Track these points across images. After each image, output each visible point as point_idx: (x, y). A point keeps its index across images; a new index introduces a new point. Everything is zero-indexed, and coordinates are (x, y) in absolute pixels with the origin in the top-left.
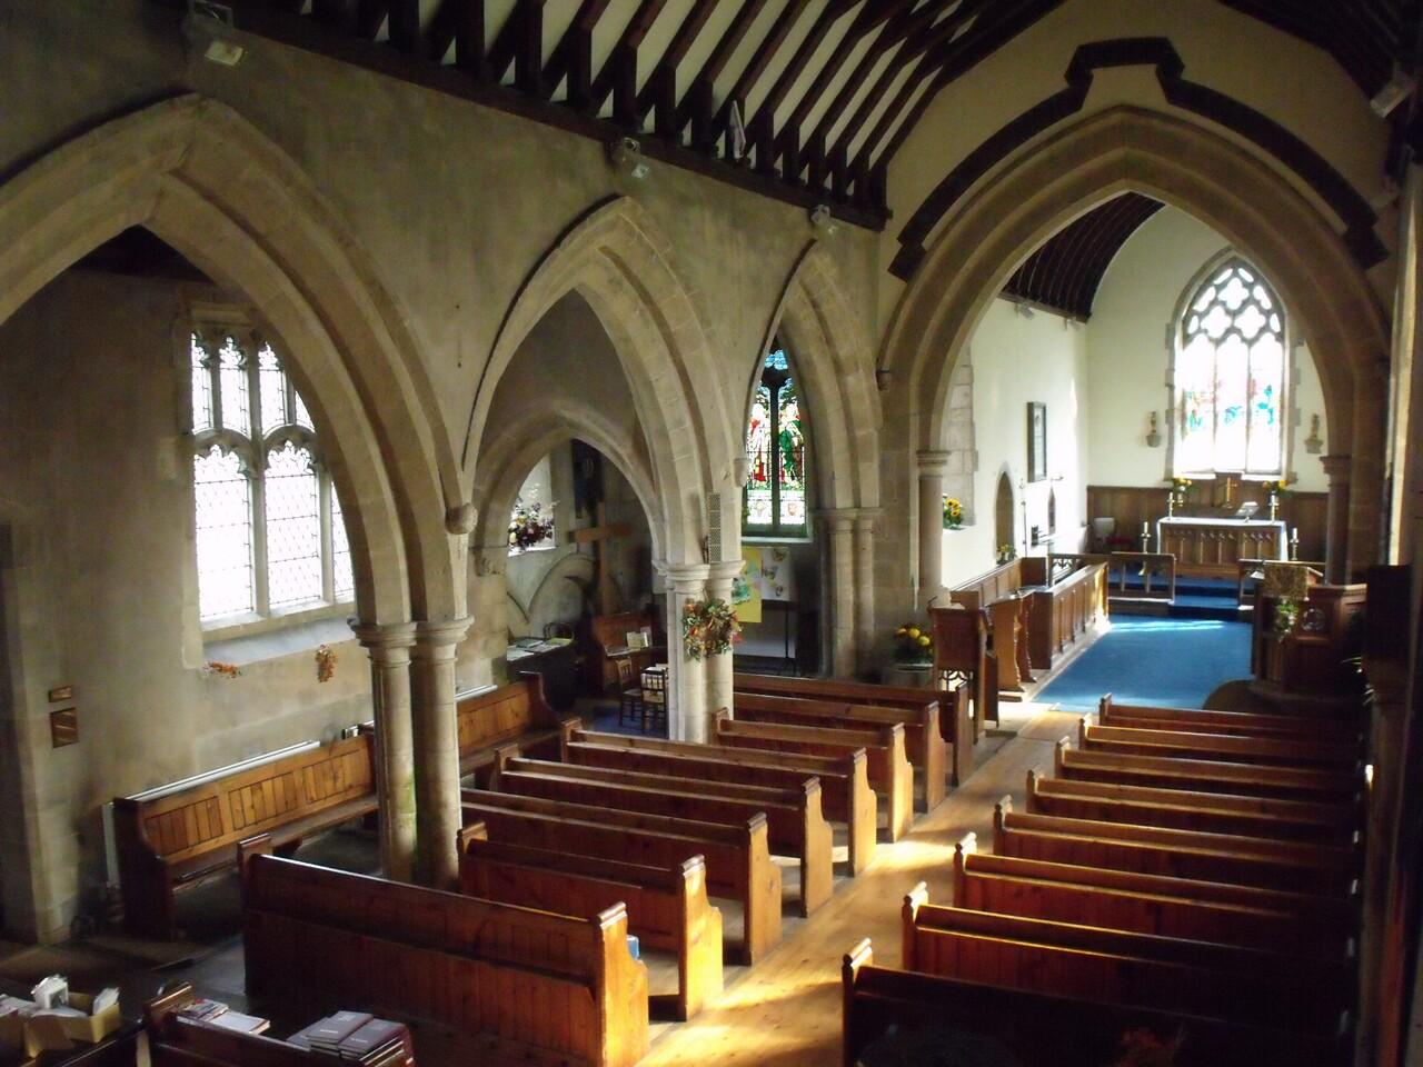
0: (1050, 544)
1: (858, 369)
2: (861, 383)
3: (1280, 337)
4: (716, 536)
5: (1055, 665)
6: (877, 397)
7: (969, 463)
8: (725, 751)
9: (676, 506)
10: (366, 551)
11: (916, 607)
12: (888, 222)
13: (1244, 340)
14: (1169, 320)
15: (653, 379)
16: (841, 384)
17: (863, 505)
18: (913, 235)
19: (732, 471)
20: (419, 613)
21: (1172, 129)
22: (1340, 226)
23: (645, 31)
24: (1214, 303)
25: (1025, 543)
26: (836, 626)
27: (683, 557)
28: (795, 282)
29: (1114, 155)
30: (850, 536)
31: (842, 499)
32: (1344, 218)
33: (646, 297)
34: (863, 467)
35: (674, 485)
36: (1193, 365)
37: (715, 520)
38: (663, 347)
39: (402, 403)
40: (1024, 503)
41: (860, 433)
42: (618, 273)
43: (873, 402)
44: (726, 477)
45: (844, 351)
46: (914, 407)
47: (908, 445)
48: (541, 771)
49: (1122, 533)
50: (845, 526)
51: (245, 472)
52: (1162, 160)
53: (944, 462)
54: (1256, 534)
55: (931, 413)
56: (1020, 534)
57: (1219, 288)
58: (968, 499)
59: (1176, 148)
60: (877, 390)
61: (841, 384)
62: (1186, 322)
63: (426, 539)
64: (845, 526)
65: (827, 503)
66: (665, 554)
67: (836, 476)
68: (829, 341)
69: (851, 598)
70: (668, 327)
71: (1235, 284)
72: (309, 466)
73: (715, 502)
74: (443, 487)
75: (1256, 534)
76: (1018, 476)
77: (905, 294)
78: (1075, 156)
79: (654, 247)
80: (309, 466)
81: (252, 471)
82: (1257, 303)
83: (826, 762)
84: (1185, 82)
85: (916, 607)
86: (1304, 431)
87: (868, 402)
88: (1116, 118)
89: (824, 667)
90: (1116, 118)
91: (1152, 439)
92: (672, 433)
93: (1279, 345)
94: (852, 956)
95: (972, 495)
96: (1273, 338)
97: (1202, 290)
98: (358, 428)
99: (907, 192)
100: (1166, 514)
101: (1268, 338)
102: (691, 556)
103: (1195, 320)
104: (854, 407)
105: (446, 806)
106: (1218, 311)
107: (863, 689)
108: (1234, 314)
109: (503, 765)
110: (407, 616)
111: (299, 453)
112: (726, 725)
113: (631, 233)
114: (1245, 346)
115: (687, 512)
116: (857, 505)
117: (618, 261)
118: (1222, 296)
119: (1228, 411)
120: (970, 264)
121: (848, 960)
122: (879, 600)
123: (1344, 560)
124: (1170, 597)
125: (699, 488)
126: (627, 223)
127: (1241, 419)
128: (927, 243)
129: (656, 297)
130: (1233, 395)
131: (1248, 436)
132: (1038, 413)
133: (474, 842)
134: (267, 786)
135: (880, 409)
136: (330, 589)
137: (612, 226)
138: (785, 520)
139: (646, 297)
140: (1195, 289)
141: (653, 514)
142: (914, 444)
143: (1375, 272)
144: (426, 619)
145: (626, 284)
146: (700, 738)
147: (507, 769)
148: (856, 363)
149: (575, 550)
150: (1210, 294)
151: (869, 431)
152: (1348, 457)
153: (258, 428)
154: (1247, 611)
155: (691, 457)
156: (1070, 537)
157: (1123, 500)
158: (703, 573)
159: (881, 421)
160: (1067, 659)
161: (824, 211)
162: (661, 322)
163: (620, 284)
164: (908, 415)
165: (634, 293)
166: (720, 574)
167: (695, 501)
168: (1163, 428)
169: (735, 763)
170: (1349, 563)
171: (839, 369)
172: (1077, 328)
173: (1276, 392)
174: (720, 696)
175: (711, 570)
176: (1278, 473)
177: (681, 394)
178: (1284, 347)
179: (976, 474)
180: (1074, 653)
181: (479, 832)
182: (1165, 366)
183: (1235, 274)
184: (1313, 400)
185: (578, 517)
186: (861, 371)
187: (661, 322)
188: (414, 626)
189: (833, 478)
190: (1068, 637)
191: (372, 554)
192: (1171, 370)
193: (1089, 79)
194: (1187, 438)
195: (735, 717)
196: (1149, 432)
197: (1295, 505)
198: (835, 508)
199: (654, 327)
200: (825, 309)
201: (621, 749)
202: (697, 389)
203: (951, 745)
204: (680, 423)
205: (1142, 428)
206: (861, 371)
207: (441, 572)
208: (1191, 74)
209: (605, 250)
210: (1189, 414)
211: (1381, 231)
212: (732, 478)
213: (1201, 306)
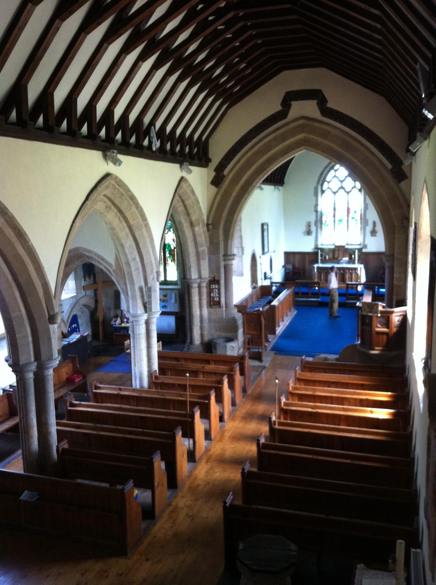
0: (271, 278)
1: (199, 224)
2: (200, 230)
3: (360, 190)
5: (277, 332)
6: (207, 235)
7: (240, 252)
8: (158, 392)
9: (133, 291)
10: (15, 335)
11: (224, 316)
12: (210, 164)
13: (346, 191)
14: (315, 185)
15: (124, 243)
17: (202, 277)
18: (220, 169)
21: (323, 126)
22: (390, 166)
23: (118, 103)
25: (262, 279)
26: (193, 325)
27: (137, 311)
28: (177, 197)
29: (302, 136)
30: (197, 289)
31: (194, 275)
32: (391, 163)
33: (120, 211)
34: (202, 262)
35: (133, 284)
36: (325, 203)
37: (150, 297)
38: (127, 230)
39: (29, 275)
40: (261, 264)
41: (200, 249)
42: (109, 203)
43: (205, 237)
44: (153, 279)
46: (221, 238)
47: (219, 254)
48: (84, 407)
49: (299, 269)
50: (195, 285)
52: (320, 139)
53: (233, 259)
54: (352, 271)
55: (228, 240)
56: (260, 276)
57: (336, 171)
58: (241, 266)
59: (325, 135)
60: (207, 232)
62: (322, 185)
63: (40, 327)
64: (195, 285)
65: (188, 277)
66: (129, 309)
67: (192, 266)
68: (188, 214)
69: (198, 313)
70: (129, 223)
73: (149, 290)
74: (47, 306)
75: (352, 271)
76: (258, 253)
77: (217, 194)
78: (284, 138)
79: (124, 193)
83: (199, 396)
84: (328, 108)
85: (224, 316)
86: (369, 228)
87: (203, 237)
89: (189, 341)
90: (301, 122)
91: (309, 233)
92: (132, 264)
93: (360, 193)
94: (227, 501)
95: (242, 265)
96: (358, 191)
97: (329, 172)
98: (11, 286)
100: (317, 262)
102: (140, 310)
103: (326, 183)
104: (198, 239)
105: (50, 434)
107: (207, 356)
108: (342, 188)
109: (68, 405)
110: (33, 359)
112: (156, 378)
113: (115, 188)
114: (346, 194)
115: (138, 293)
116: (200, 277)
117: (110, 199)
119: (340, 220)
121: (225, 503)
122: (209, 313)
123: (392, 295)
124: (319, 298)
125: (143, 284)
126: (113, 185)
128: (226, 172)
129: (124, 211)
130: (341, 213)
131: (335, 204)
132: (265, 227)
133: (64, 449)
135: (208, 239)
137: (107, 187)
138: (168, 279)
139: (120, 211)
140: (326, 172)
141: (123, 293)
142: (222, 252)
143: (403, 184)
144: (41, 360)
145: (113, 207)
146: (146, 383)
147: (70, 407)
148: (199, 222)
149: (84, 294)
151: (204, 249)
152: (393, 255)
154: (222, 29)
155: (139, 272)
156: (278, 276)
157: (297, 257)
158: (145, 317)
159: (208, 244)
160: (282, 329)
161: (186, 165)
162: (127, 221)
163: (110, 208)
164: (219, 241)
165: (116, 210)
166: (152, 316)
167: (141, 289)
168: (313, 228)
169: (162, 397)
170: (394, 297)
171: (192, 225)
172: (279, 190)
175: (148, 315)
176: (360, 245)
177: (135, 248)
179: (243, 257)
180: (284, 325)
181: (65, 445)
182: (314, 203)
184: (373, 215)
185: (85, 280)
186: (201, 225)
187: (127, 221)
188: (36, 363)
189: (190, 267)
190: (281, 319)
191: (17, 336)
192: (317, 205)
193: (290, 105)
194: (323, 231)
195: (159, 374)
197: (365, 257)
198: (191, 279)
199: (124, 223)
200: (187, 202)
201: (115, 392)
202: (141, 246)
203: (243, 377)
204: (134, 259)
205: (304, 228)
206: (201, 225)
207: (47, 341)
208: (330, 105)
209: (105, 196)
210: (324, 222)
212: (156, 279)
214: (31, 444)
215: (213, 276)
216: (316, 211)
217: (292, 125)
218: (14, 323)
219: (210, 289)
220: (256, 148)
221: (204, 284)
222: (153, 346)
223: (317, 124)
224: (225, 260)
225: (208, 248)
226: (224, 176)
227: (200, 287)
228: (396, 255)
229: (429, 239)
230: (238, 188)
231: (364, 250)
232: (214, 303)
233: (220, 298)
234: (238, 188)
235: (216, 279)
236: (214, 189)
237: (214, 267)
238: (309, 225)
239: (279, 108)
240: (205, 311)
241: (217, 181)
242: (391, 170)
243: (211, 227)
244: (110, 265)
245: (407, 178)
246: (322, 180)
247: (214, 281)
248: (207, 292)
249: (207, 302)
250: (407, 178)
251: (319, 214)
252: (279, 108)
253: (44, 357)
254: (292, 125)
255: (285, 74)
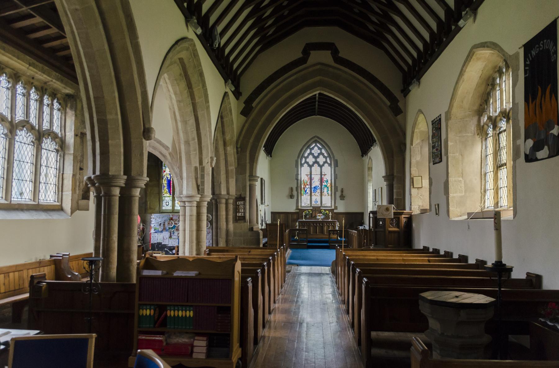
3: (330, 165)
4: (203, 183)
6: (236, 156)
16: (225, 150)
18: (249, 102)
19: (210, 161)
20: (127, 171)
22: (389, 103)
24: (309, 154)
29: (318, 78)
32: (137, 280)
34: (230, 180)
45: (228, 137)
51: (6, 135)
61: (225, 150)
64: (224, 201)
69: (225, 227)
71: (316, 148)
72: (32, 142)
80: (32, 142)
81: (9, 134)
82: (323, 154)
86: (339, 194)
88: (318, 67)
90: (318, 67)
91: (291, 196)
97: (306, 149)
99: (249, 84)
101: (326, 165)
104: (229, 159)
106: (311, 156)
111: (28, 134)
116: (228, 193)
118: (313, 152)
120: (268, 113)
122: (235, 228)
125: (198, 165)
127: (319, 191)
129: (193, 86)
130: (316, 182)
134: (11, 275)
136: (37, 196)
140: (304, 149)
143: (399, 117)
150: (308, 151)
151: (232, 168)
153: (14, 116)
168: (295, 193)
173: (329, 182)
174: (202, 247)
178: (331, 168)
183: (316, 145)
191: (110, 142)
196: (290, 194)
205: (287, 192)
211: (400, 104)
213: (306, 155)
214: (110, 271)
215: (239, 194)
216: (297, 180)
217: (311, 69)
218: (109, 126)
219: (236, 205)
220: (279, 87)
221: (231, 201)
222: (203, 229)
223: (331, 70)
224: (250, 180)
225: (236, 169)
226: (253, 107)
227: (227, 204)
228: (395, 174)
229: (552, 19)
230: (263, 118)
231: (335, 211)
232: (240, 219)
233: (245, 213)
234: (263, 118)
235: (243, 196)
236: (243, 118)
237: (241, 186)
238: (292, 189)
239: (300, 55)
240: (231, 226)
241: (246, 112)
242: (390, 106)
243: (239, 150)
244: (167, 148)
245: (402, 112)
246: (301, 155)
247: (240, 198)
248: (234, 208)
249: (233, 218)
250: (402, 112)
251: (299, 181)
252: (300, 55)
253: (134, 173)
254: (311, 69)
255: (306, 30)
